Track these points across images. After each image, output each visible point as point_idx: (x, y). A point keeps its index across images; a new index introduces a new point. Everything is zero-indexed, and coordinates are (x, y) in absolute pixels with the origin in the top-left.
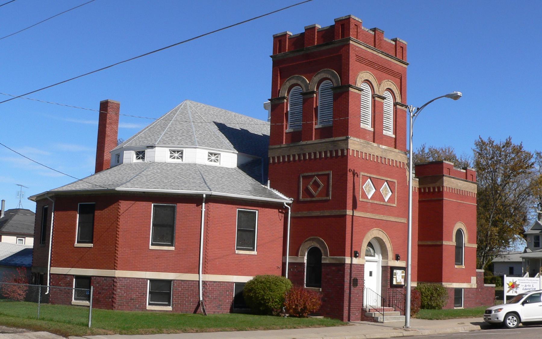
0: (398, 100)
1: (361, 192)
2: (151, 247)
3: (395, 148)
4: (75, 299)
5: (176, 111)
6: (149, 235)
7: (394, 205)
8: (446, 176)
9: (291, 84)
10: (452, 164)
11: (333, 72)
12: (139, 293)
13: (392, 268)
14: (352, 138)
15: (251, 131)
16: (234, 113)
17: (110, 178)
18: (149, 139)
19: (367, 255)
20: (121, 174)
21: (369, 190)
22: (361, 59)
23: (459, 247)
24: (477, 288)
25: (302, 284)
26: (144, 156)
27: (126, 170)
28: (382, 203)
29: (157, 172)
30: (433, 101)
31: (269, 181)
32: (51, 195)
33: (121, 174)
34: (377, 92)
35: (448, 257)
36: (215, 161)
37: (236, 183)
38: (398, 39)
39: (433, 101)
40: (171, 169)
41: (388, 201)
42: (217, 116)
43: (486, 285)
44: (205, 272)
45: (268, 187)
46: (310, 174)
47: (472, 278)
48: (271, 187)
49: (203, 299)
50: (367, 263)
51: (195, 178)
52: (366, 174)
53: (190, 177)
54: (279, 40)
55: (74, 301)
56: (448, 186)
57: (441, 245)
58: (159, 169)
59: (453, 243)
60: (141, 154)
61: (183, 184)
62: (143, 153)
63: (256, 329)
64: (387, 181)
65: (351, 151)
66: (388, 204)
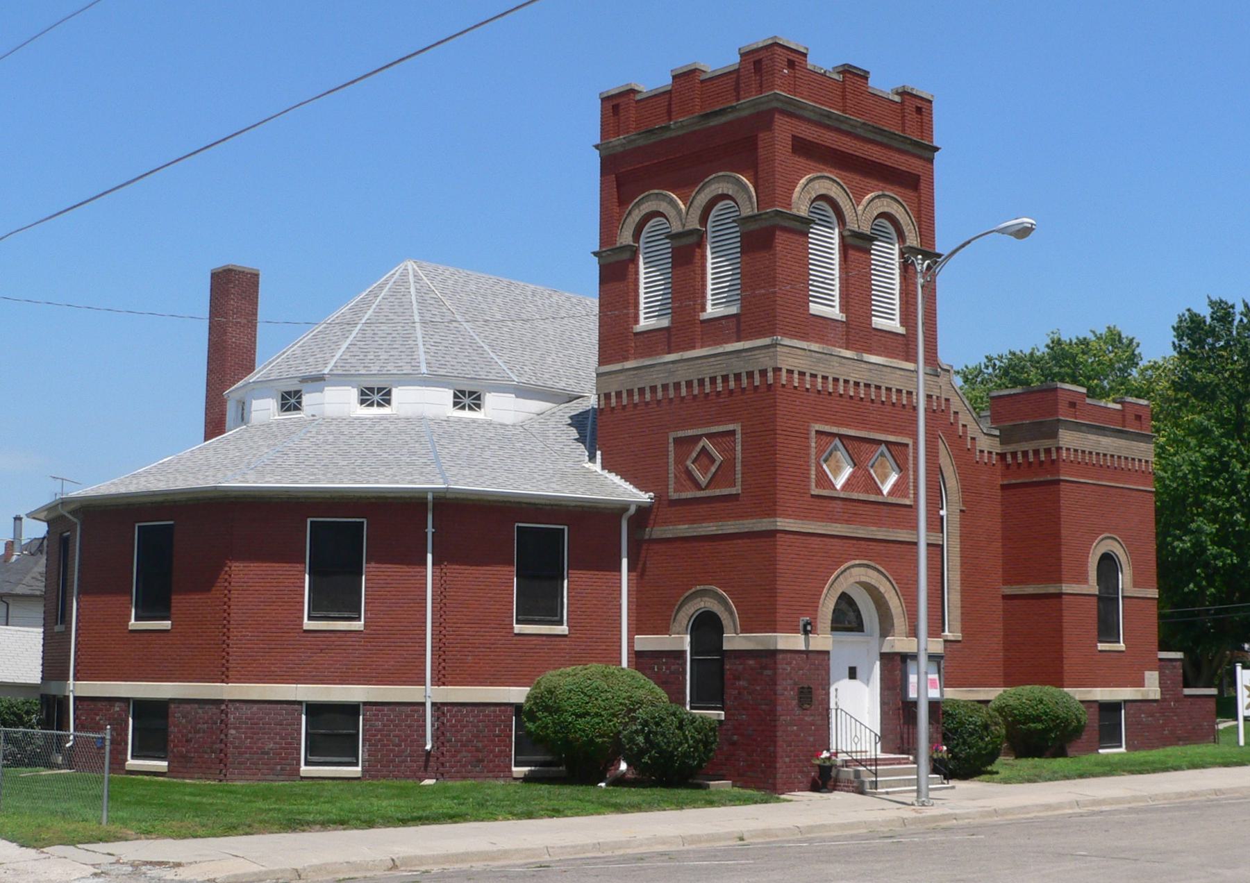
0: (913, 240)
1: (813, 472)
2: (308, 624)
5: (381, 287)
6: (303, 595)
9: (644, 213)
10: (1084, 390)
11: (738, 180)
12: (282, 738)
16: (532, 287)
17: (213, 462)
18: (311, 360)
20: (240, 450)
23: (1107, 599)
24: (1163, 700)
25: (684, 705)
26: (300, 403)
27: (256, 439)
28: (872, 498)
29: (325, 442)
30: (969, 242)
31: (599, 453)
32: (72, 507)
33: (240, 450)
35: (1078, 625)
37: (518, 460)
39: (969, 242)
40: (360, 434)
41: (891, 493)
42: (484, 296)
43: (1187, 691)
44: (439, 680)
46: (690, 433)
47: (1147, 674)
48: (603, 468)
51: (414, 453)
52: (827, 428)
53: (405, 451)
54: (617, 106)
58: (331, 433)
59: (1092, 586)
60: (291, 401)
61: (382, 469)
62: (297, 394)
63: (492, 817)
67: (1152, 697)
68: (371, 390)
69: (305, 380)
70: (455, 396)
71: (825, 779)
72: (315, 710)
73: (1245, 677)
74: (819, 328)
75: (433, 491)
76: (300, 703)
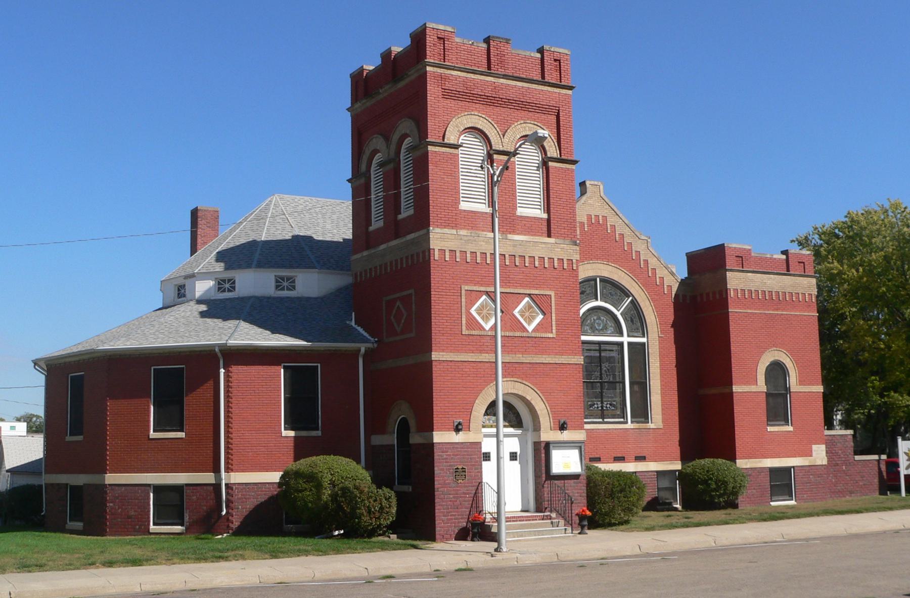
0: (553, 152)
3: (549, 236)
4: (154, 524)
7: (550, 335)
8: (731, 270)
13: (547, 445)
14: (438, 230)
15: (318, 237)
19: (484, 427)
21: (485, 316)
22: (448, 94)
28: (525, 334)
34: (497, 146)
36: (288, 289)
38: (546, 47)
45: (353, 323)
47: (814, 447)
49: (227, 513)
50: (485, 439)
55: (152, 527)
56: (746, 288)
57: (731, 394)
64: (529, 295)
65: (437, 253)
66: (538, 335)
67: (819, 463)
68: (224, 281)
69: (187, 277)
70: (277, 281)
71: (478, 530)
72: (159, 490)
73: (903, 446)
74: (471, 220)
75: (219, 345)
76: (149, 485)
